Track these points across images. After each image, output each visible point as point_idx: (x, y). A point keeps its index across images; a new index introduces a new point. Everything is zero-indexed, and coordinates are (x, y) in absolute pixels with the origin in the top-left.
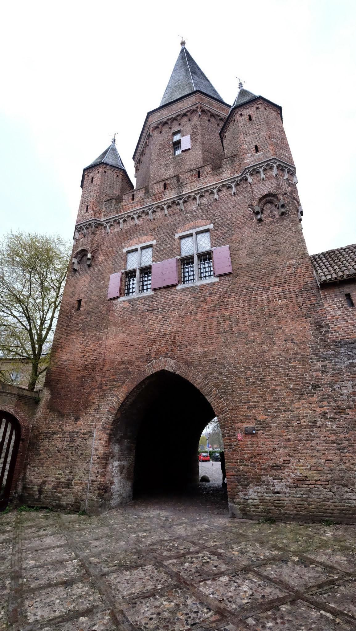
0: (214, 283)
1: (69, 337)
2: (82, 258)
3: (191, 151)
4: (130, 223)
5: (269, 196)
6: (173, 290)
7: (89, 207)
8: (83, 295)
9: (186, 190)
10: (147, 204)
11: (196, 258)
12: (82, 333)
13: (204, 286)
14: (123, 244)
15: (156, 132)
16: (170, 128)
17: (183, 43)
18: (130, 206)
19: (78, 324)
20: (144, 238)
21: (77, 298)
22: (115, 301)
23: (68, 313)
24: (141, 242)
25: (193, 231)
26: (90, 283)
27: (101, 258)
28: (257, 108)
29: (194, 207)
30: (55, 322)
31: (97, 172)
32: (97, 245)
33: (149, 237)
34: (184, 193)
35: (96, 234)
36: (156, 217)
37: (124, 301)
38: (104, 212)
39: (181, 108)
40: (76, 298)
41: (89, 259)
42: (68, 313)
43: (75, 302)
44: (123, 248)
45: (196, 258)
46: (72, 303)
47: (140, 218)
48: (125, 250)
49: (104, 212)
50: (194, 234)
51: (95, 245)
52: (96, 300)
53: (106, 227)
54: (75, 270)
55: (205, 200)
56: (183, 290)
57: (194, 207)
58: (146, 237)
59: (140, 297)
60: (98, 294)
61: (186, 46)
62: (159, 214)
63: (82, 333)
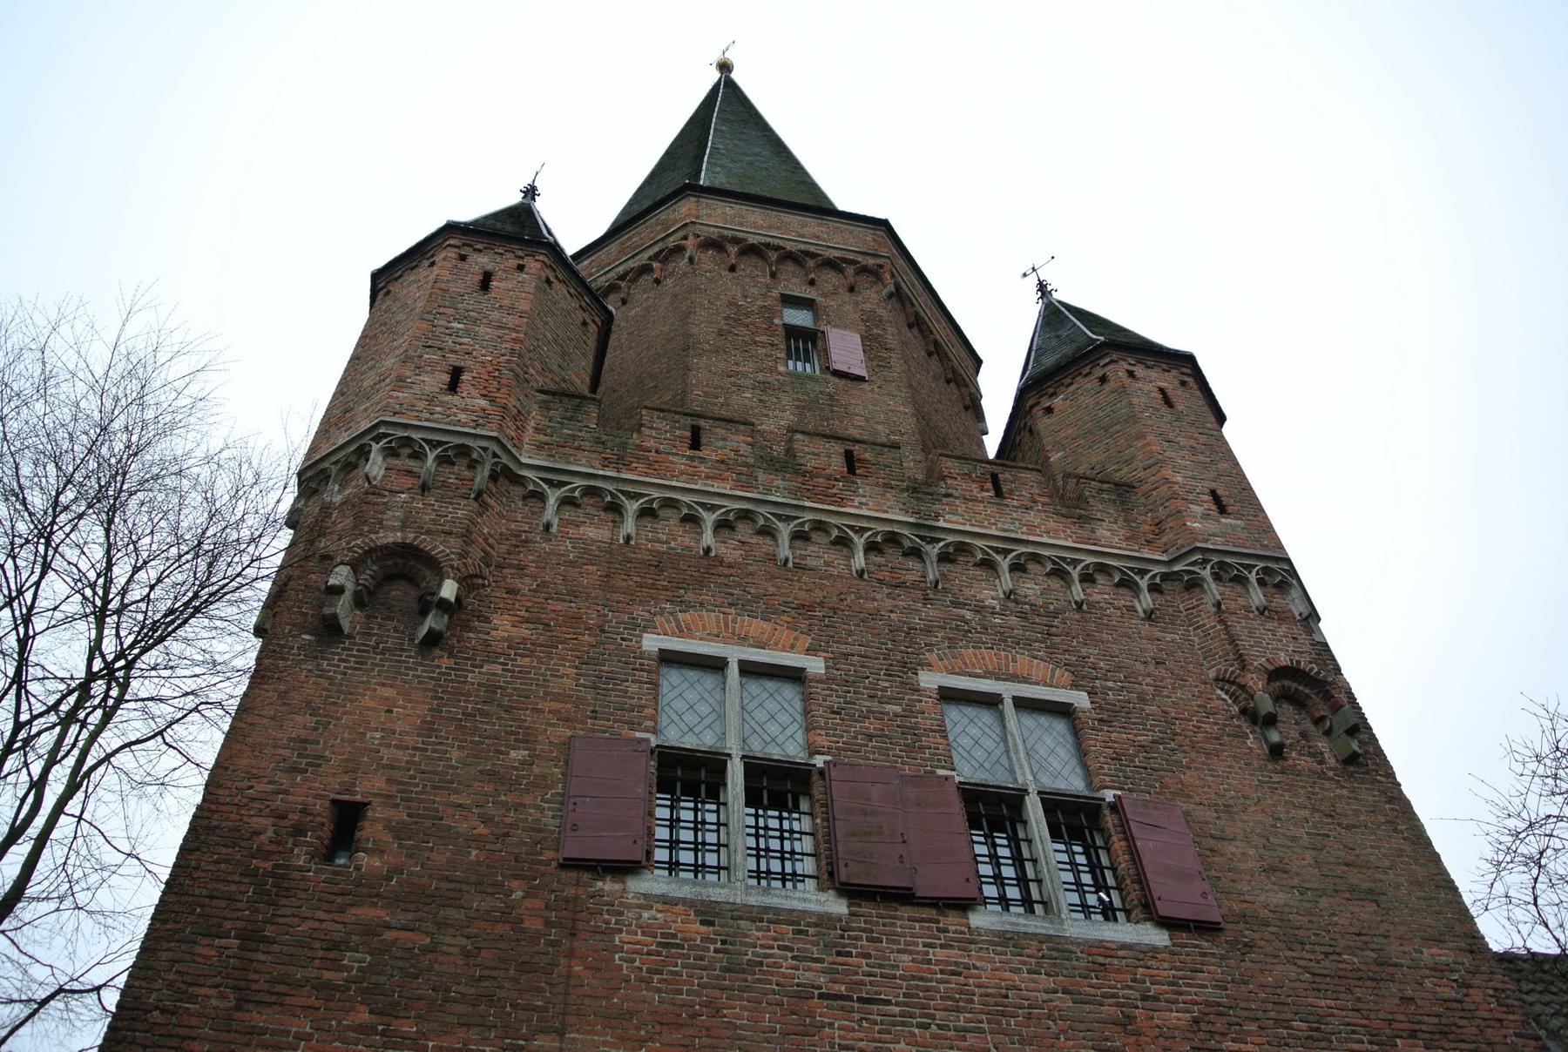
0: (1153, 951)
1: (258, 1018)
2: (379, 585)
3: (865, 386)
4: (669, 535)
5: (1285, 677)
6: (951, 921)
7: (465, 377)
8: (379, 783)
9: (953, 520)
10: (768, 491)
11: (736, 775)
12: (364, 1016)
13: (1102, 948)
14: (639, 612)
15: (707, 259)
16: (773, 275)
17: (725, 67)
18: (680, 463)
19: (335, 946)
20: (757, 627)
21: (335, 783)
22: (608, 886)
23: (265, 855)
24: (743, 640)
25: (1007, 690)
26: (427, 729)
27: (503, 626)
28: (1103, 380)
29: (990, 595)
30: (1356, 1046)
31: (514, 262)
32: (486, 559)
33: (785, 635)
34: (941, 524)
35: (484, 506)
36: (811, 562)
37: (668, 901)
38: (538, 430)
39: (818, 237)
40: (329, 783)
41: (443, 605)
42: (265, 855)
43: (321, 806)
44: (649, 627)
45: (736, 775)
46: (297, 799)
47: (726, 533)
48: (651, 643)
49: (538, 430)
50: (734, 669)
51: (476, 553)
52: (476, 840)
53: (540, 497)
54: (330, 630)
55: (1031, 588)
56: (1007, 940)
57: (990, 595)
58: (768, 626)
59: (767, 909)
60: (491, 809)
61: (733, 75)
62: (818, 554)
63: (364, 1016)
